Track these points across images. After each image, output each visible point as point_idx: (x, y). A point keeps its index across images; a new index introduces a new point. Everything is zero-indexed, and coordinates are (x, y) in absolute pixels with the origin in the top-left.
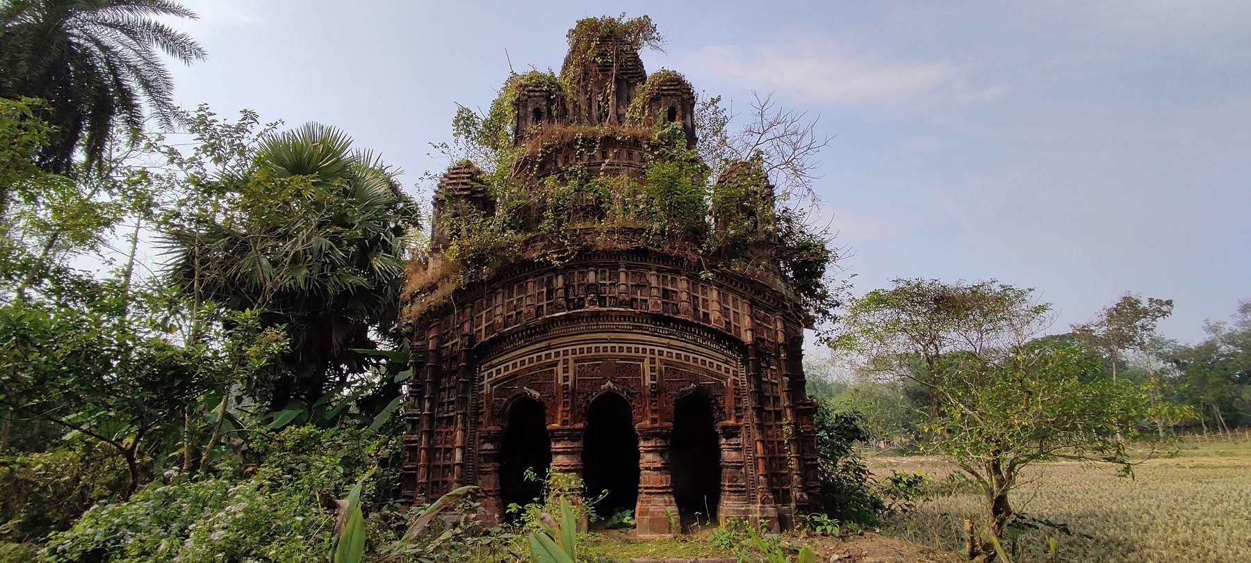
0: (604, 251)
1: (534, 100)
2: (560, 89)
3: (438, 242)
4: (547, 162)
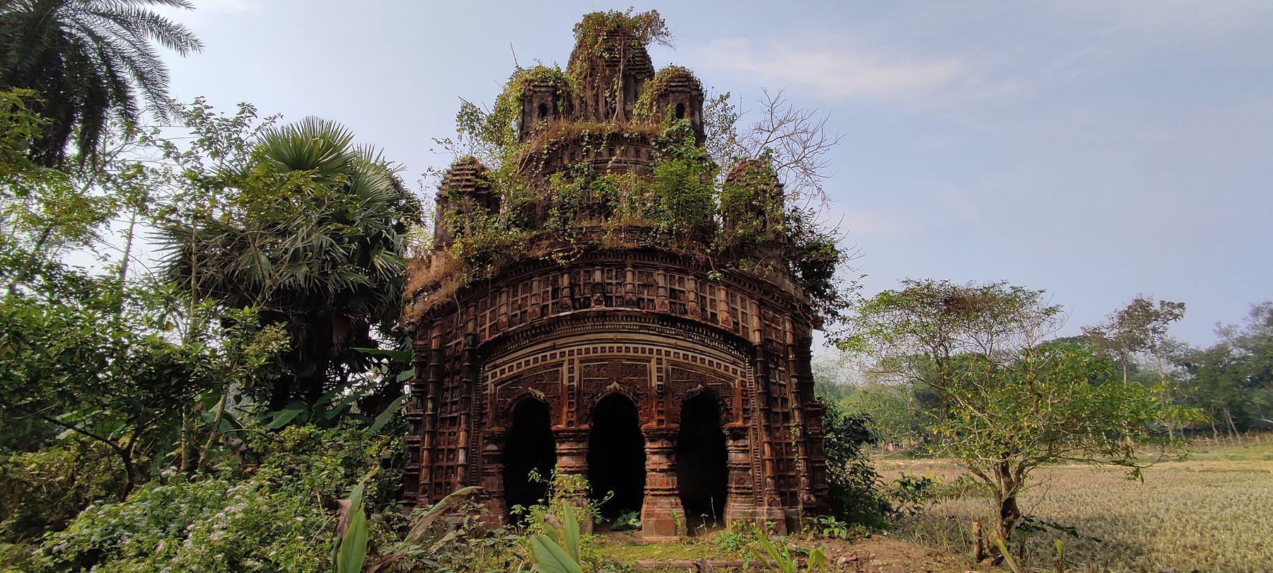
0: (610, 249)
1: (540, 96)
2: (566, 84)
3: (442, 240)
4: (553, 159)
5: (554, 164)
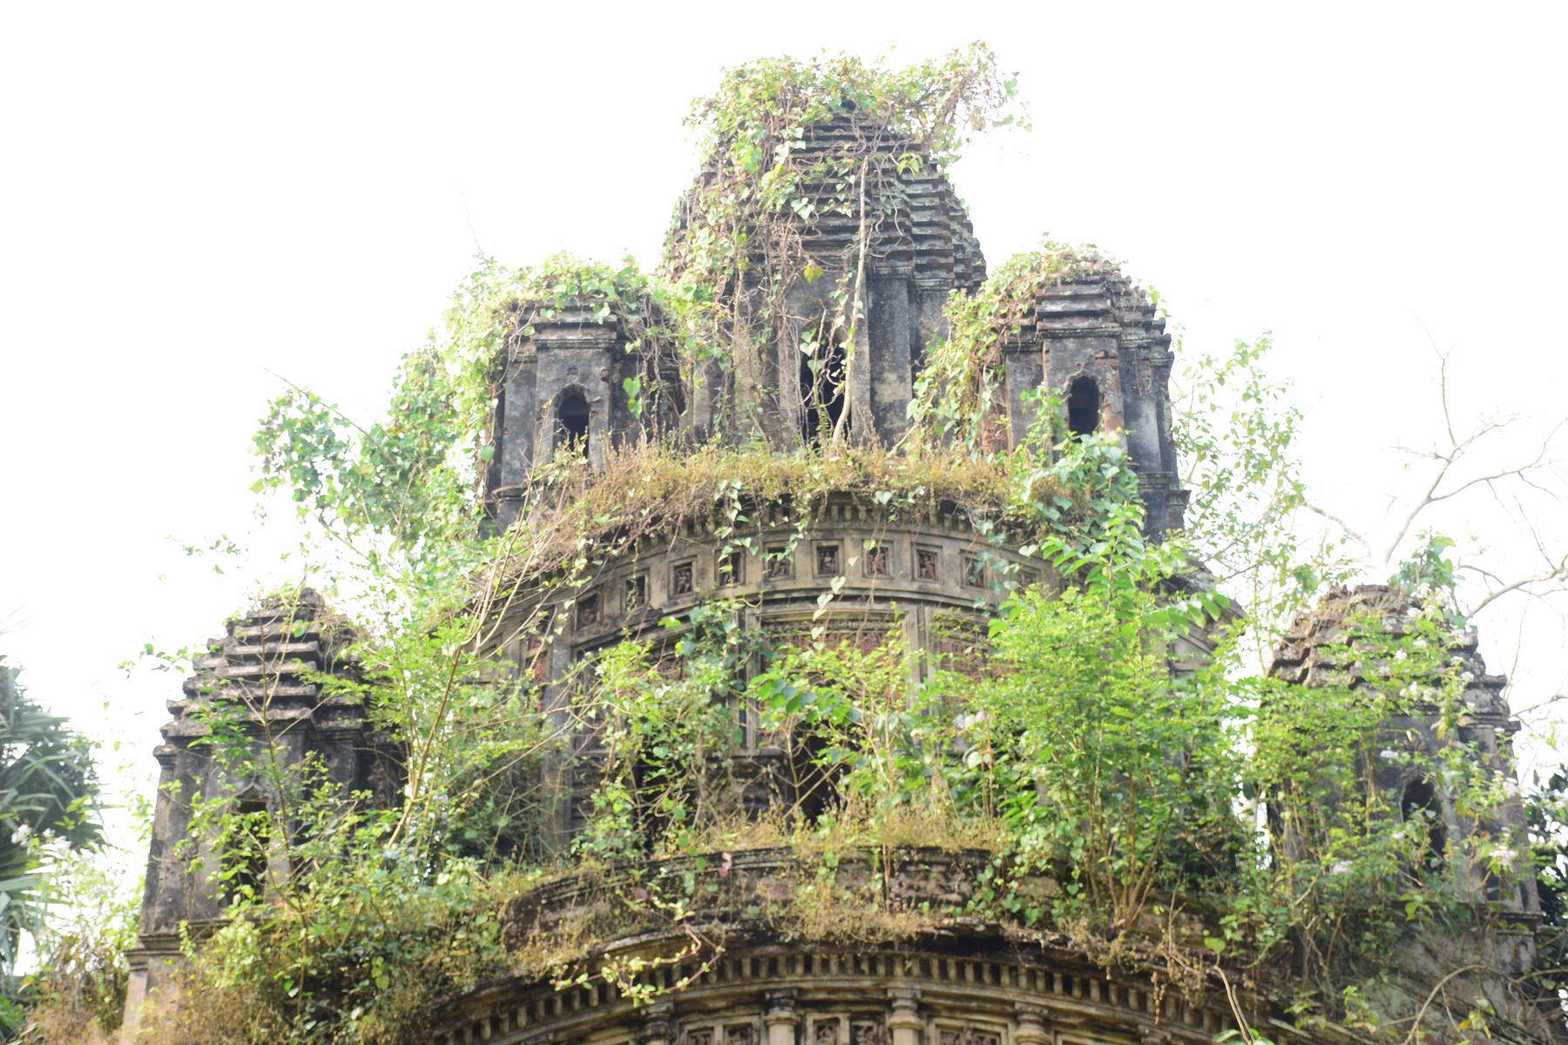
0: (828, 942)
1: (582, 369)
2: (658, 316)
3: (174, 911)
4: (601, 597)
5: (610, 607)
